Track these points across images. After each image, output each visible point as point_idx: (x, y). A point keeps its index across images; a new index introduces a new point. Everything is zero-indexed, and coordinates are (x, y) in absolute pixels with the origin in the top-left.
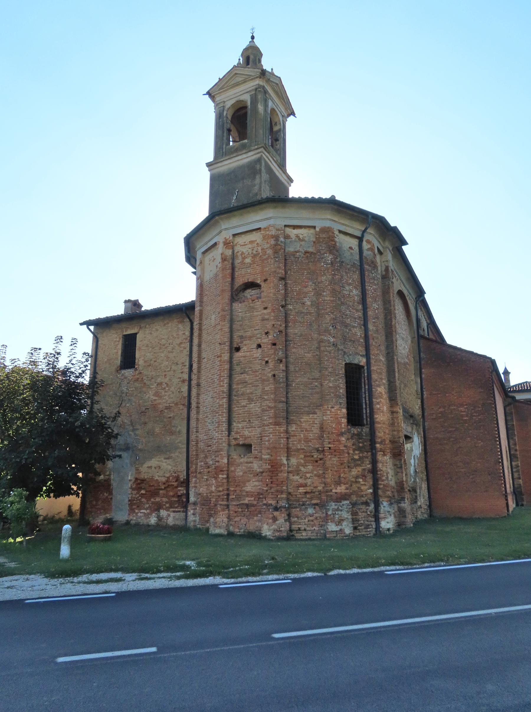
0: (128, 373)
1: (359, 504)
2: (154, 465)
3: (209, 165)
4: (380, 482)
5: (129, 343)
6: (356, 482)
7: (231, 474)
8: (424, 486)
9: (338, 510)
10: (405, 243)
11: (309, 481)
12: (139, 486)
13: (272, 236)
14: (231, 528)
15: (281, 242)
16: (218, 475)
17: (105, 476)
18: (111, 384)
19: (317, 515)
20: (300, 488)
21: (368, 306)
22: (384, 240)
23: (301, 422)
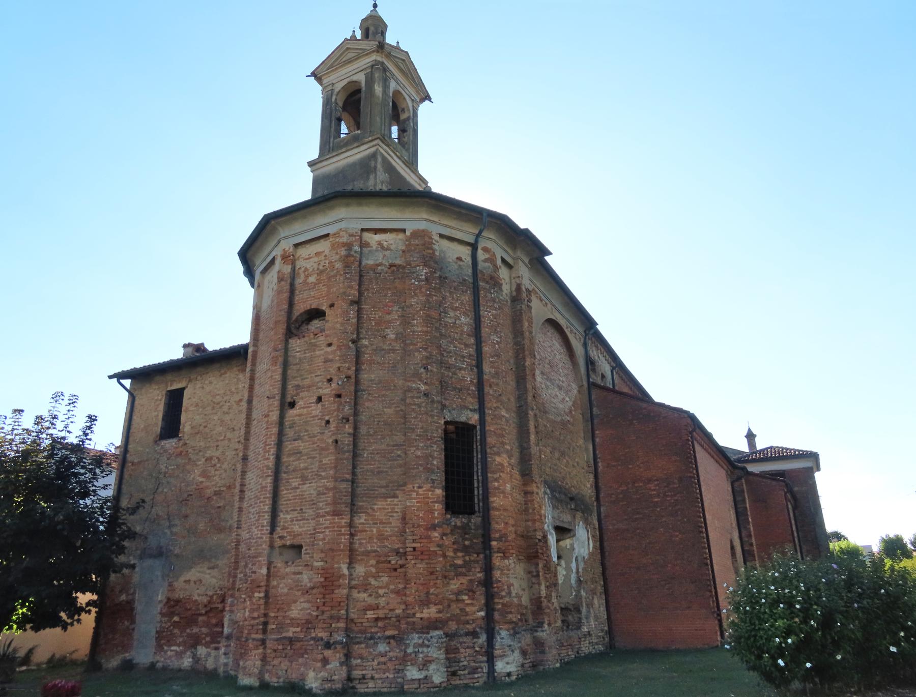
0: (170, 444)
1: (461, 636)
2: (193, 579)
3: (311, 164)
4: (496, 600)
5: (175, 400)
6: (458, 600)
7: (272, 592)
8: (599, 603)
9: (422, 645)
10: (549, 253)
11: (382, 601)
12: (172, 610)
13: (344, 245)
14: (267, 677)
15: (356, 252)
16: (253, 593)
17: (128, 595)
18: (147, 460)
19: (391, 654)
20: (368, 612)
21: (483, 339)
22: (514, 248)
23: (373, 509)
